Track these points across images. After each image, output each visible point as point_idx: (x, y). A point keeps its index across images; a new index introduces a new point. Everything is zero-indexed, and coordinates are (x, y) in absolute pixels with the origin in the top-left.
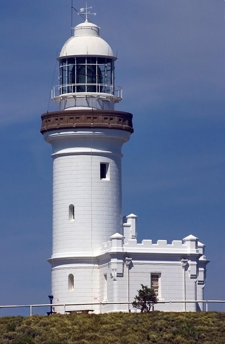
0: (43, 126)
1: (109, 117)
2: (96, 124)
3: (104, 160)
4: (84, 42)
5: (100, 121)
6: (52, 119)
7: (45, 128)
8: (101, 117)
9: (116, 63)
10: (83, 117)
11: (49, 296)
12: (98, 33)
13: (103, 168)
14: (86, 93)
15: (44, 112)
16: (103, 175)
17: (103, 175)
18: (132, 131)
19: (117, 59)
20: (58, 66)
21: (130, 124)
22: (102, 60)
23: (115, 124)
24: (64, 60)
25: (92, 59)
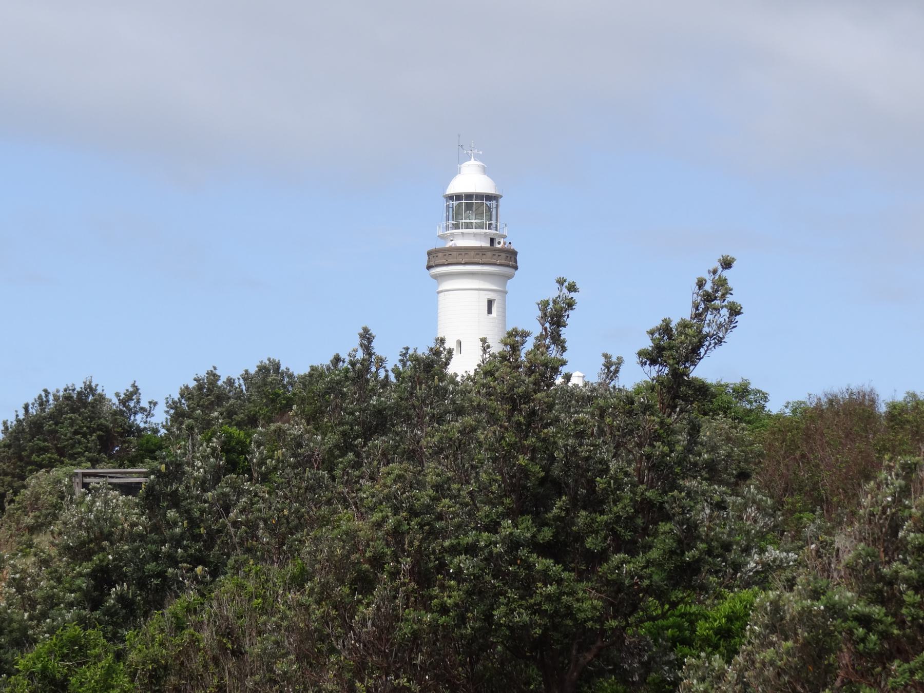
0: (429, 262)
1: (497, 254)
2: (485, 260)
3: (491, 296)
4: (470, 179)
5: (488, 257)
6: (440, 255)
7: (432, 263)
8: (504, 255)
9: (501, 201)
10: (454, 253)
11: (366, 330)
12: (485, 171)
13: (490, 303)
14: (474, 230)
15: (432, 248)
16: (490, 311)
17: (490, 311)
18: (516, 268)
19: (501, 197)
20: (443, 203)
21: (516, 262)
22: (489, 197)
23: (503, 262)
24: (451, 197)
25: (480, 196)
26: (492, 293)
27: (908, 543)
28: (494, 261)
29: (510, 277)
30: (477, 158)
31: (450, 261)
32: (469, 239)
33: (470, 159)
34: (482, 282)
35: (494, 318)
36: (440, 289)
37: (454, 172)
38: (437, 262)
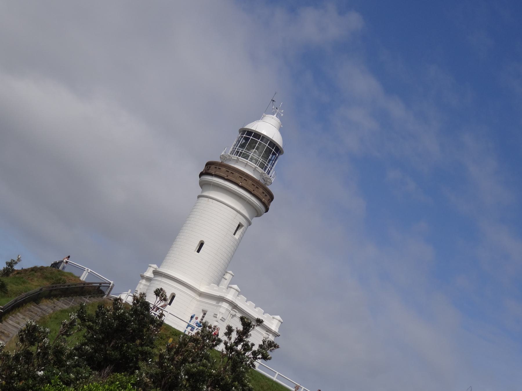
1: (266, 193)
4: (268, 127)
6: (224, 169)
10: (237, 174)
12: (281, 130)
13: (239, 226)
18: (267, 210)
26: (244, 220)
27: (212, 335)
28: (261, 197)
29: (258, 214)
30: (278, 116)
31: (229, 177)
32: (248, 167)
33: (273, 115)
34: (245, 210)
35: (235, 239)
36: (206, 194)
37: (258, 117)
38: (218, 173)
